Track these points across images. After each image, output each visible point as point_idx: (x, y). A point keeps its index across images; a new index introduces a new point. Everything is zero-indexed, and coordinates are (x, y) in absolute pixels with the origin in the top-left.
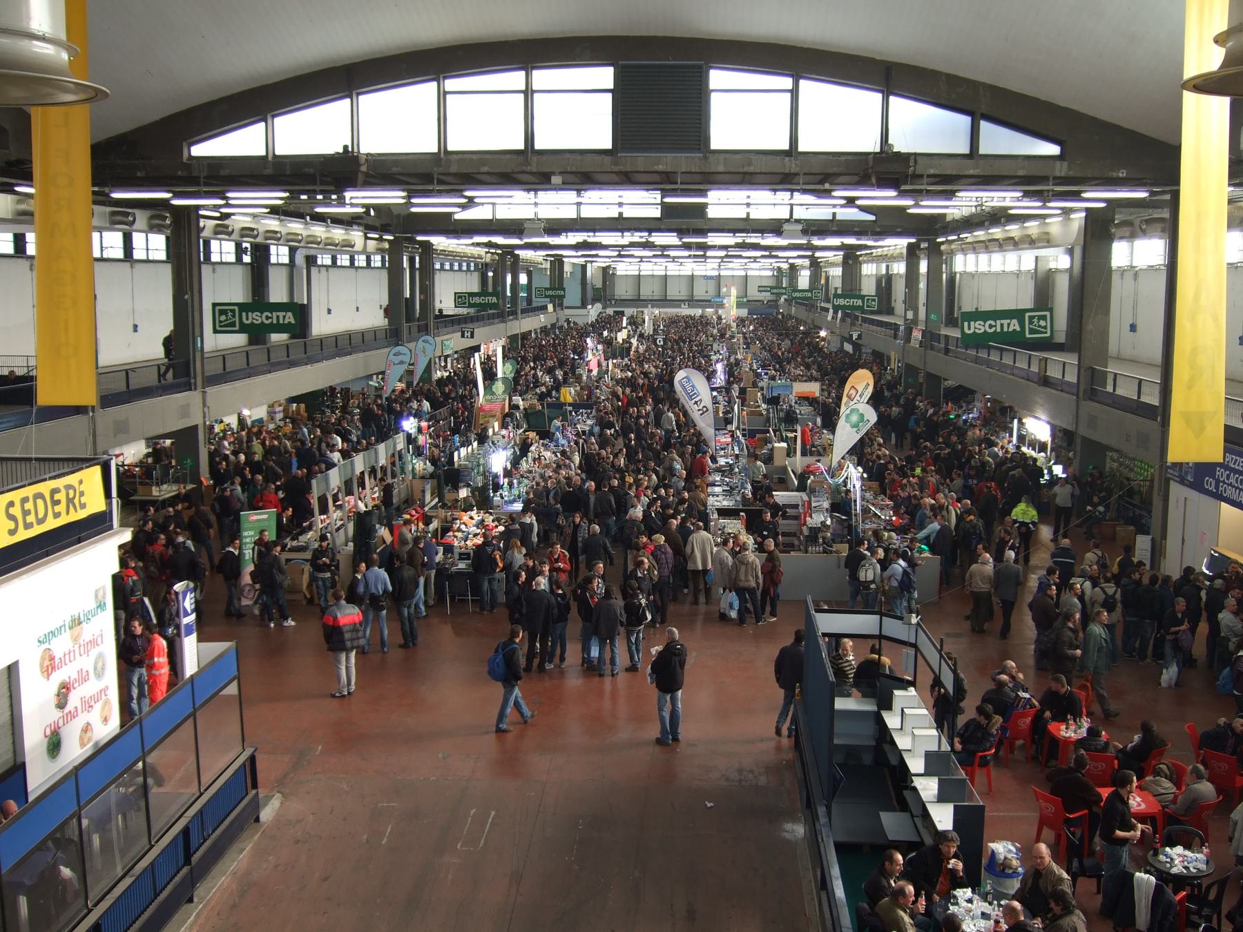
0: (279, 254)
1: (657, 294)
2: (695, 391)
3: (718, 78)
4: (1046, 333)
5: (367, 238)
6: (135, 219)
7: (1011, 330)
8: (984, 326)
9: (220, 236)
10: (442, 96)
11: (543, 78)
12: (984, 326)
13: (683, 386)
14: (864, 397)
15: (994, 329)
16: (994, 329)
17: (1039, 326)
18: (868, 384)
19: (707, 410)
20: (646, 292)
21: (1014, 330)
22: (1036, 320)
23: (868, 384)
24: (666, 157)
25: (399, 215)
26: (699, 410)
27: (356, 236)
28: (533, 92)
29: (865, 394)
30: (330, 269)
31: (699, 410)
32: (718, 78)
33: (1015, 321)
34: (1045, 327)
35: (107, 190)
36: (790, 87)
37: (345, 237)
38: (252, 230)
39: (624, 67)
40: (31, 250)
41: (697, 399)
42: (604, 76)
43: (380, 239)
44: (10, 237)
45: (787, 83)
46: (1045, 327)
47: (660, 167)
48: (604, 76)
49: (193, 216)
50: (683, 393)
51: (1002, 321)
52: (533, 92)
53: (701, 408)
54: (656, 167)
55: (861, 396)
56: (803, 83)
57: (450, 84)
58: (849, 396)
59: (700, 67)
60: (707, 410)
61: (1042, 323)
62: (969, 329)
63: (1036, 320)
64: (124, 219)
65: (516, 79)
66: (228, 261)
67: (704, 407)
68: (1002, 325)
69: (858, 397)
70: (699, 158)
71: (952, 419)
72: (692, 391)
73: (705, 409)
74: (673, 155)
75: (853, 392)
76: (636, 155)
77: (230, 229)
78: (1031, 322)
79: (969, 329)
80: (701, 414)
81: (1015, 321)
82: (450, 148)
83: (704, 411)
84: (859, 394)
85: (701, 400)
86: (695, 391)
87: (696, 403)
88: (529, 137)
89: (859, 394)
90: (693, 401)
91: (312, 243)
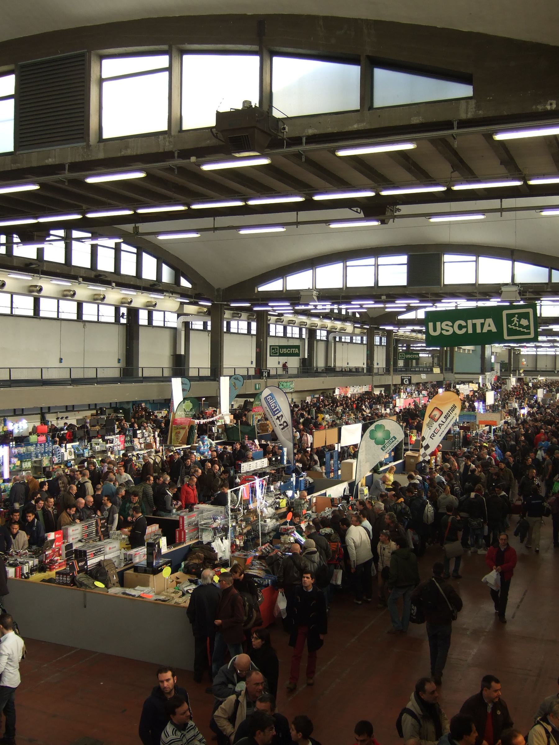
0: (321, 335)
1: (549, 367)
2: (278, 407)
3: (447, 258)
4: (529, 334)
5: (355, 327)
6: (241, 316)
7: (485, 330)
8: (452, 327)
9: (290, 325)
10: (345, 268)
11: (382, 260)
12: (452, 327)
13: (267, 402)
14: (450, 418)
15: (464, 330)
16: (464, 330)
17: (521, 326)
18: (454, 407)
19: (287, 425)
20: (541, 365)
21: (490, 331)
22: (515, 319)
23: (454, 407)
24: (55, 150)
25: (218, 290)
26: (281, 425)
27: (349, 327)
28: (375, 265)
29: (451, 416)
30: (379, 347)
31: (281, 425)
32: (447, 258)
33: (490, 321)
34: (528, 327)
35: (229, 303)
36: (475, 260)
37: (342, 326)
38: (293, 321)
39: (411, 255)
40: (209, 328)
41: (279, 415)
42: (404, 259)
43: (361, 328)
44: (202, 323)
45: (474, 258)
46: (528, 327)
47: (50, 160)
48: (404, 259)
49: (265, 314)
50: (268, 409)
51: (474, 321)
52: (378, 265)
53: (282, 423)
54: (47, 161)
55: (446, 417)
56: (481, 259)
57: (349, 263)
58: (431, 417)
59: (439, 254)
60: (287, 425)
61: (524, 322)
62: (435, 330)
63: (515, 319)
64: (238, 316)
65: (371, 261)
66: (246, 327)
67: (285, 422)
68: (474, 326)
69: (442, 418)
70: (83, 148)
71: (536, 453)
72: (275, 407)
73: (285, 424)
74: (59, 147)
75: (437, 413)
76: (30, 151)
77: (282, 320)
78: (509, 322)
79: (435, 330)
80: (282, 429)
81: (490, 321)
82: (348, 286)
83: (285, 426)
84: (443, 415)
85: (282, 416)
86: (278, 407)
87: (278, 418)
88: (377, 282)
89: (443, 415)
90: (276, 417)
91: (323, 328)
